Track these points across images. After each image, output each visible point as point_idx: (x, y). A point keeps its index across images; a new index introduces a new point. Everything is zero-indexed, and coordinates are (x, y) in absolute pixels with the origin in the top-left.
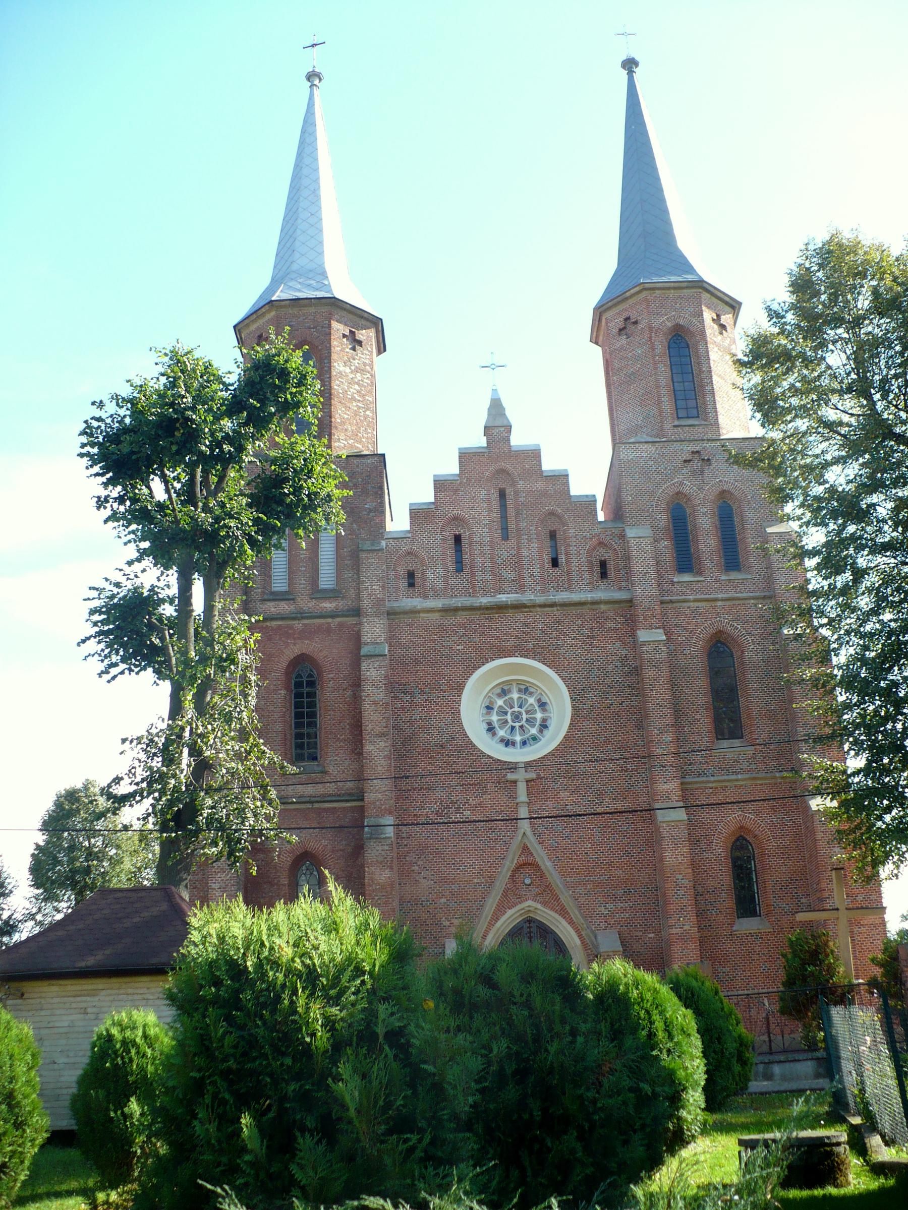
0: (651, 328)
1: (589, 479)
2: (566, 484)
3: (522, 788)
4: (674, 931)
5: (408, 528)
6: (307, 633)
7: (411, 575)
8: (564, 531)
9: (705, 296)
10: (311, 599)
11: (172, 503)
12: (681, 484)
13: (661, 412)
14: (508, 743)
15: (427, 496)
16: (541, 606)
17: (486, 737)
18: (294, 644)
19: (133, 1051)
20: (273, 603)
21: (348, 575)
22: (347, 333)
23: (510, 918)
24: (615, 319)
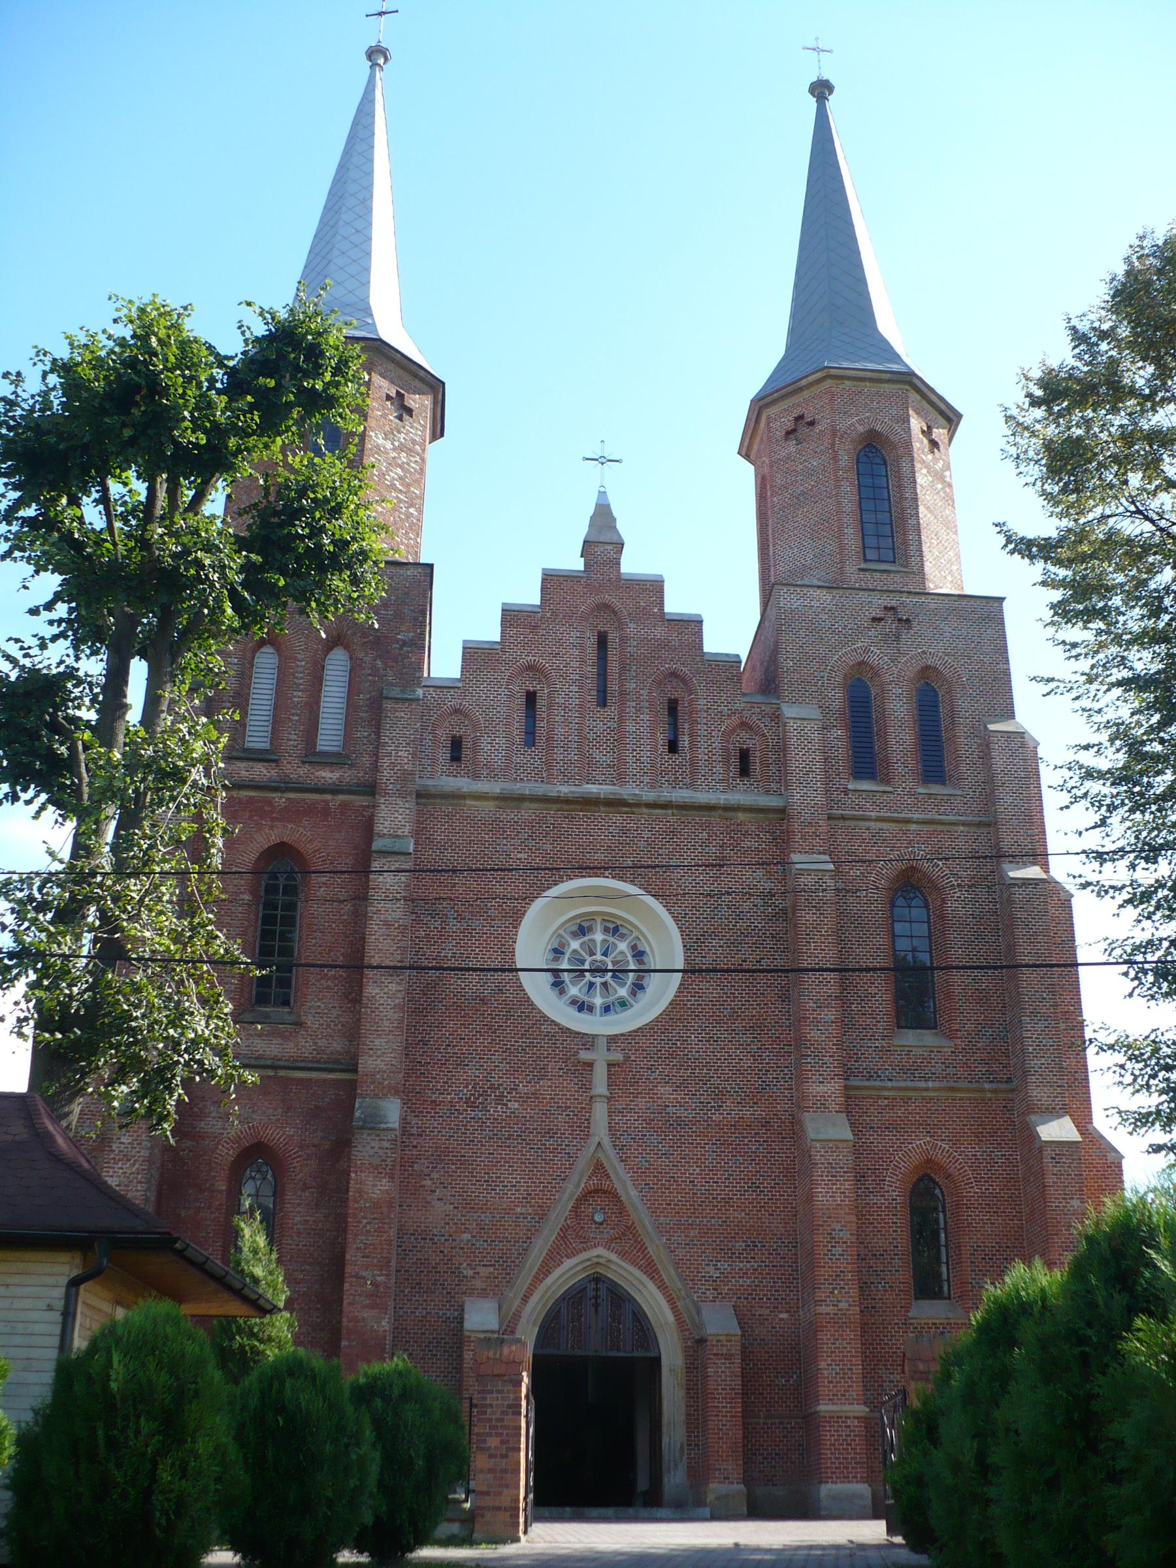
0: (834, 432)
1: (731, 626)
3: (600, 1075)
4: (823, 1309)
5: (458, 676)
6: (293, 813)
7: (456, 746)
9: (914, 396)
10: (304, 762)
11: (112, 534)
12: (867, 650)
14: (582, 1007)
15: (491, 632)
16: (649, 805)
17: (552, 995)
18: (271, 828)
21: (362, 733)
22: (393, 394)
23: (567, 1273)
24: (779, 424)
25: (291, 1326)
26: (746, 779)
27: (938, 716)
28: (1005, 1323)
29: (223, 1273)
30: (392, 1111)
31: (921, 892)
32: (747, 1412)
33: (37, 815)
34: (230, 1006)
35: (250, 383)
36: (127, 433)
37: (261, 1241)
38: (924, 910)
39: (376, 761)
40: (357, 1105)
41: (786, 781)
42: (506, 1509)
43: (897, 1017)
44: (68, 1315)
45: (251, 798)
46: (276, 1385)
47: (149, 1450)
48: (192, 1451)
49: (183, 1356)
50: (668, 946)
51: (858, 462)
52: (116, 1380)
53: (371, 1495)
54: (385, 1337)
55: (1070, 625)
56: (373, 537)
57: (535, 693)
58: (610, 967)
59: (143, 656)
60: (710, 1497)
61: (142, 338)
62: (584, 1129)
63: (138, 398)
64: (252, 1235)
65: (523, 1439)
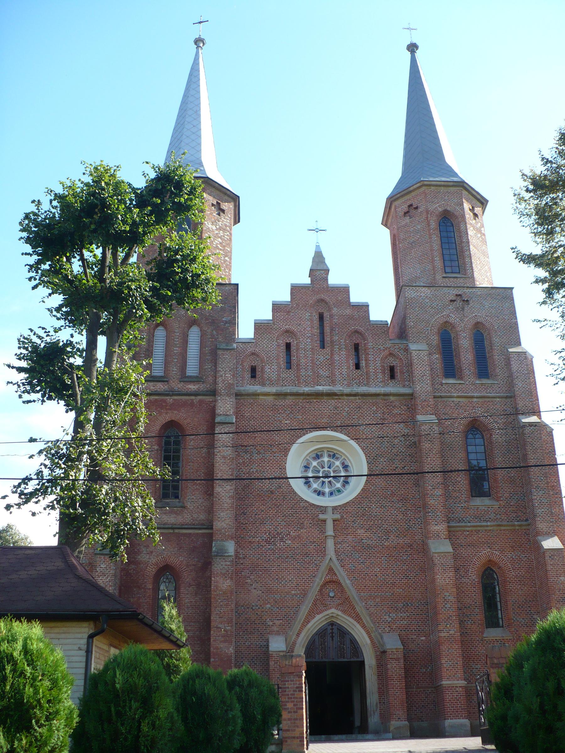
0: (427, 212)
1: (383, 310)
2: (367, 312)
4: (442, 634)
6: (175, 406)
7: (253, 370)
8: (365, 344)
9: (465, 192)
10: (180, 381)
11: (86, 276)
12: (448, 316)
13: (434, 267)
14: (319, 493)
15: (267, 315)
17: (305, 488)
19: (8, 668)
20: (152, 384)
21: (208, 366)
22: (215, 203)
23: (317, 622)
24: (401, 208)
25: (188, 652)
26: (393, 380)
29: (161, 629)
30: (231, 547)
32: (407, 686)
35: (149, 201)
36: (93, 227)
37: (174, 612)
38: (482, 440)
40: (213, 545)
41: (413, 381)
42: (297, 738)
43: (471, 492)
44: (89, 652)
45: (156, 400)
46: (191, 682)
47: (137, 717)
48: (157, 716)
49: (150, 670)
50: (360, 463)
51: (439, 225)
52: (119, 683)
53: (239, 735)
54: (231, 656)
57: (290, 343)
58: (332, 474)
59: (103, 333)
61: (97, 182)
62: (323, 552)
63: (97, 210)
64: (169, 610)
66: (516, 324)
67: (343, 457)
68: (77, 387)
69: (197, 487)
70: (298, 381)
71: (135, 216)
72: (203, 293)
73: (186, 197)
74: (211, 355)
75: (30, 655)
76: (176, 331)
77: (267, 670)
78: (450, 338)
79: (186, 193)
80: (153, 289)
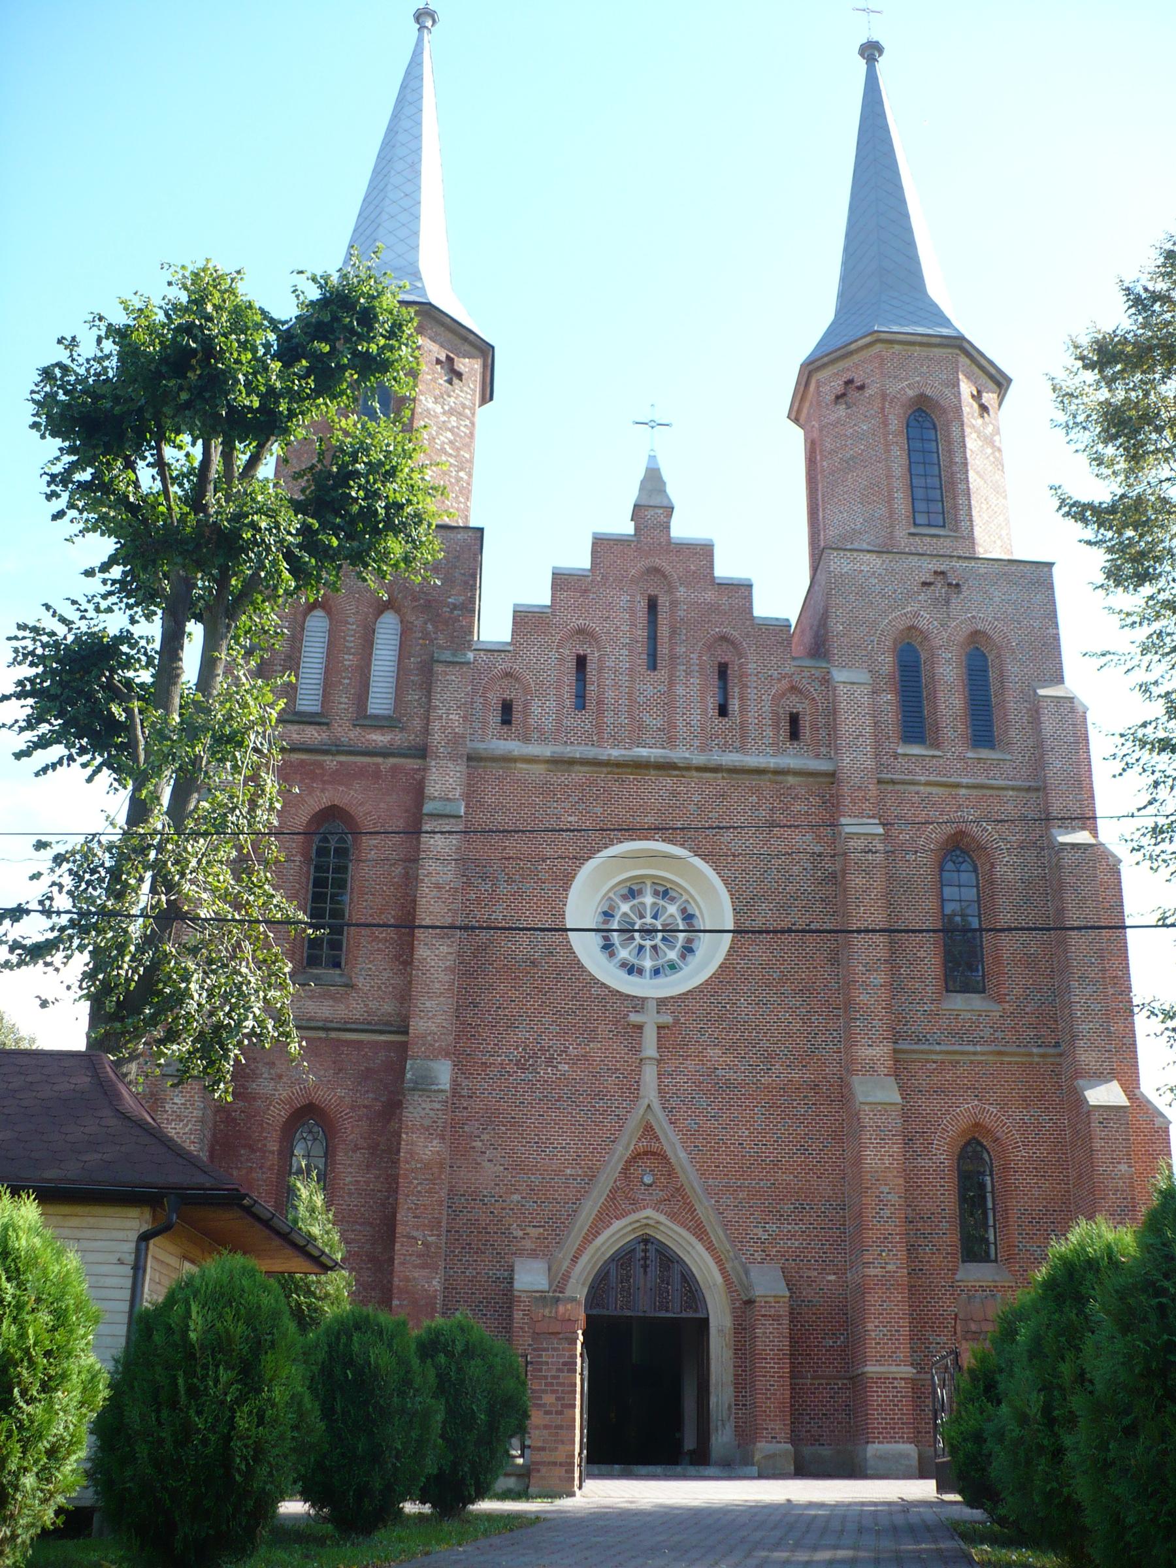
0: (884, 396)
2: (749, 598)
4: (872, 1271)
5: (509, 640)
6: (342, 776)
7: (507, 709)
9: (963, 360)
10: (355, 726)
11: (167, 498)
12: (916, 615)
13: (891, 513)
14: (632, 969)
15: (541, 595)
16: (699, 769)
17: (602, 957)
21: (413, 696)
22: (443, 358)
23: (616, 1235)
24: (830, 386)
25: (349, 1284)
27: (987, 681)
28: (1074, 1281)
29: (288, 1230)
30: (444, 1073)
31: (970, 857)
32: (794, 1374)
33: (90, 780)
34: (290, 965)
35: (304, 348)
36: (184, 396)
38: (973, 875)
39: (428, 725)
40: (408, 1067)
41: (836, 745)
42: (561, 1465)
44: (138, 1269)
45: (302, 761)
46: (344, 1339)
48: (269, 1399)
49: (259, 1307)
50: (716, 906)
51: (908, 426)
52: (195, 1330)
54: (435, 1297)
55: (1121, 589)
56: (428, 499)
59: (199, 618)
60: (757, 1457)
61: (198, 301)
62: (633, 1090)
63: (194, 362)
65: (578, 1396)
66: (1056, 638)
67: (685, 897)
68: (139, 727)
69: (380, 945)
70: (598, 734)
71: (274, 377)
72: (407, 542)
73: (382, 342)
74: (419, 674)
75: (13, 1260)
76: (351, 620)
77: (508, 1329)
78: (918, 661)
79: (383, 336)
80: (305, 530)
